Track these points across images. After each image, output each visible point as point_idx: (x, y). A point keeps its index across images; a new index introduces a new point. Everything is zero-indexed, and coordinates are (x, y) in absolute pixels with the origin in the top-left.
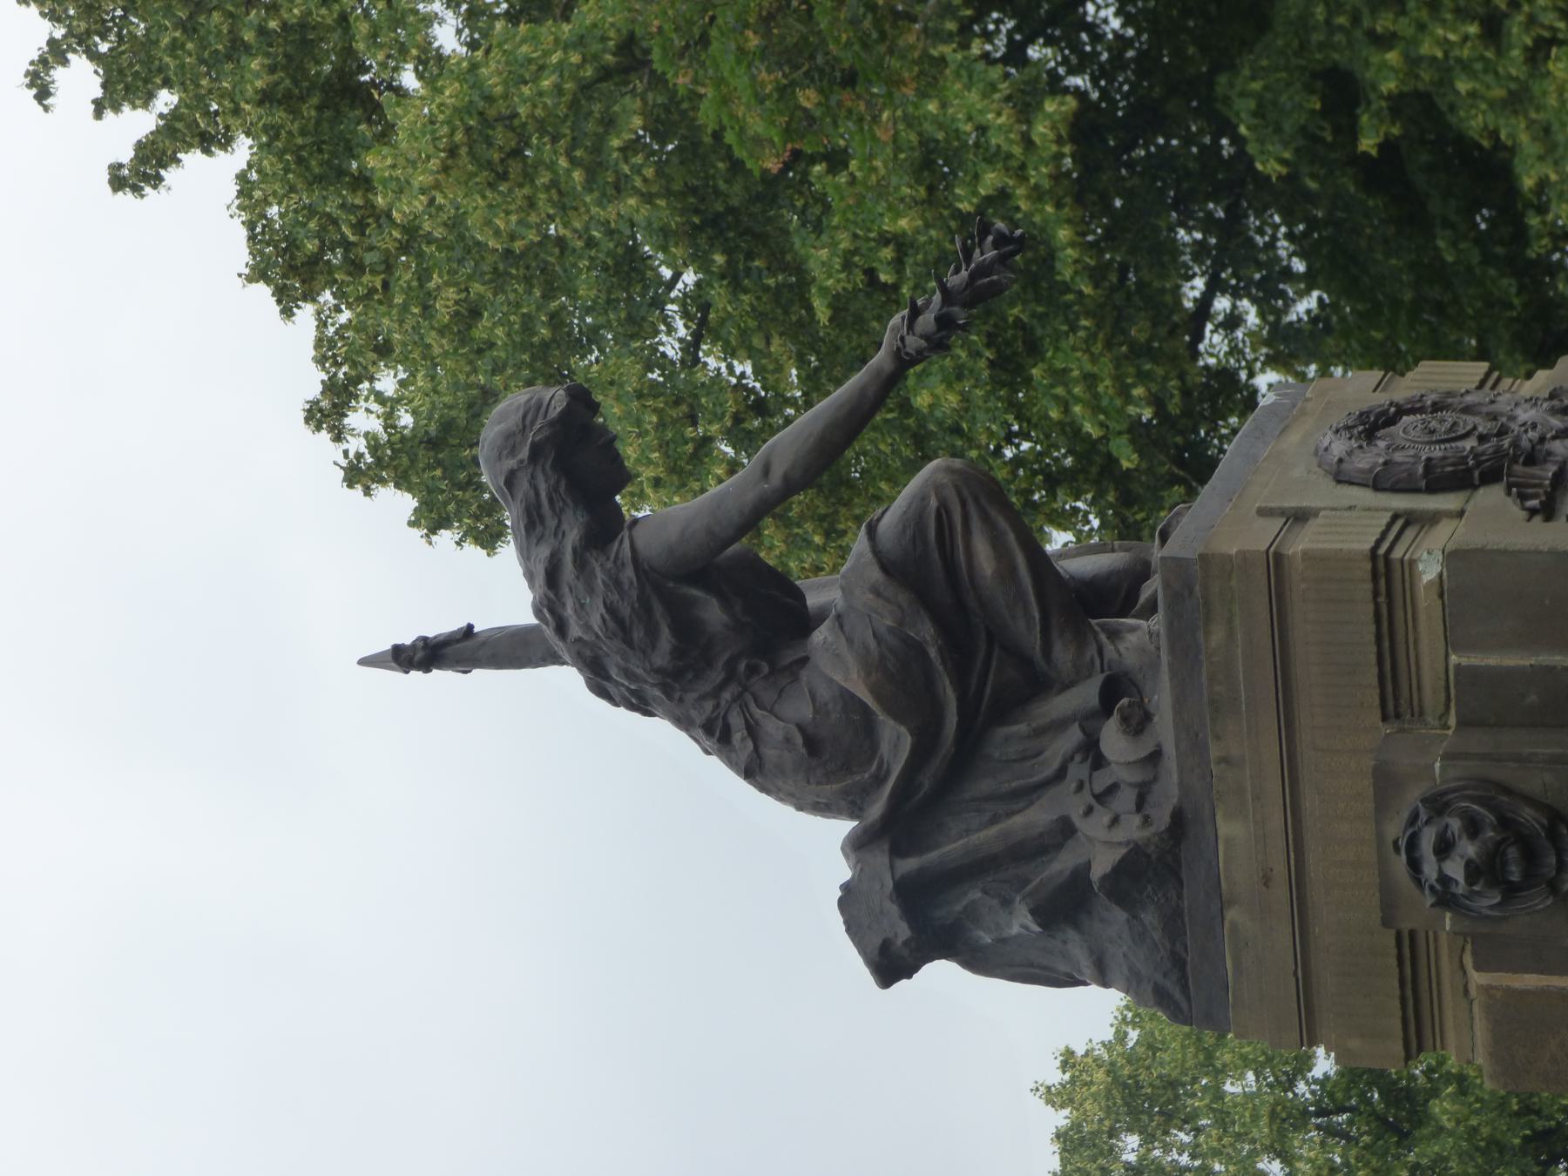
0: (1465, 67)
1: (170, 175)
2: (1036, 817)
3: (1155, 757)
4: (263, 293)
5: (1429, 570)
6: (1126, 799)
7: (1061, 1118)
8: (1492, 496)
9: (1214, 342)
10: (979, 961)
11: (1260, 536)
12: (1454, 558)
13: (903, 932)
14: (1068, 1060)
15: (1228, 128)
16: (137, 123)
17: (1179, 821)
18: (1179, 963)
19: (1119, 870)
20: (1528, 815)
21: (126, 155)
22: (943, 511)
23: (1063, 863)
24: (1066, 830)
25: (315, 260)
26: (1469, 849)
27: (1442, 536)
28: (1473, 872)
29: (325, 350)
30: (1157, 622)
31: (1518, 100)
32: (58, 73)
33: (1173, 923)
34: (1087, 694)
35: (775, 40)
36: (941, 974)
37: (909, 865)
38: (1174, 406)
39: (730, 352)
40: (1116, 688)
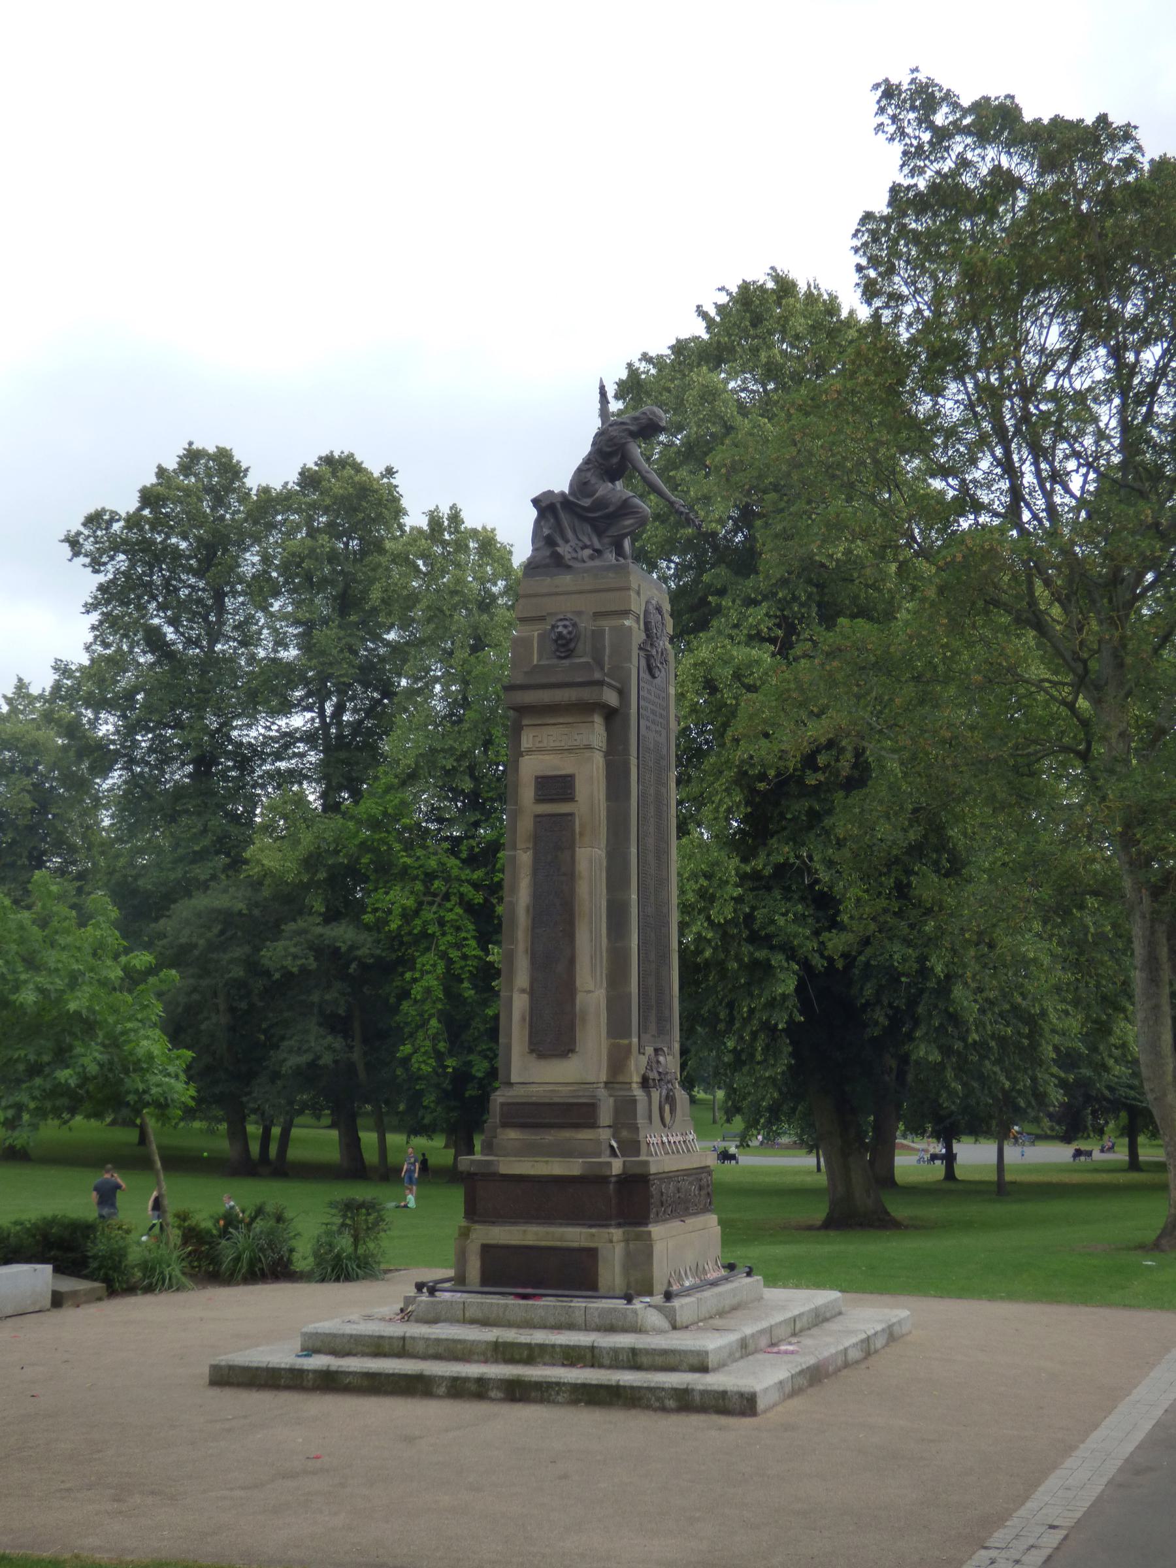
0: (727, 620)
1: (700, 318)
2: (570, 534)
3: (584, 561)
4: (674, 342)
5: (627, 623)
6: (574, 555)
7: (480, 529)
8: (643, 636)
9: (664, 564)
10: (537, 522)
11: (634, 586)
12: (630, 628)
13: (544, 505)
14: (493, 530)
15: (713, 566)
16: (712, 312)
17: (569, 567)
18: (537, 567)
19: (558, 554)
20: (572, 645)
21: (705, 309)
22: (637, 513)
23: (560, 541)
24: (567, 541)
25: (682, 354)
26: (565, 632)
27: (635, 625)
28: (560, 633)
29: (660, 357)
30: (614, 561)
31: (720, 632)
32: (724, 293)
33: (546, 566)
34: (598, 546)
35: (1164, 836)
36: (533, 513)
37: (559, 506)
38: (650, 555)
39: (661, 452)
40: (599, 552)
